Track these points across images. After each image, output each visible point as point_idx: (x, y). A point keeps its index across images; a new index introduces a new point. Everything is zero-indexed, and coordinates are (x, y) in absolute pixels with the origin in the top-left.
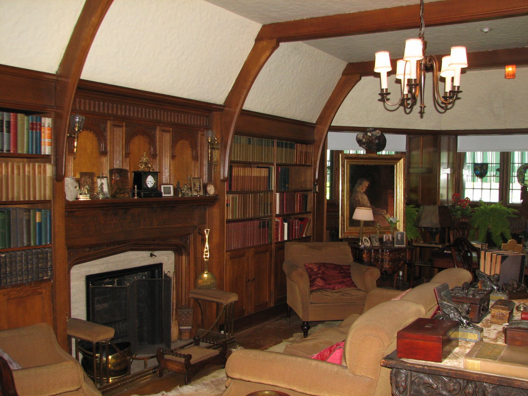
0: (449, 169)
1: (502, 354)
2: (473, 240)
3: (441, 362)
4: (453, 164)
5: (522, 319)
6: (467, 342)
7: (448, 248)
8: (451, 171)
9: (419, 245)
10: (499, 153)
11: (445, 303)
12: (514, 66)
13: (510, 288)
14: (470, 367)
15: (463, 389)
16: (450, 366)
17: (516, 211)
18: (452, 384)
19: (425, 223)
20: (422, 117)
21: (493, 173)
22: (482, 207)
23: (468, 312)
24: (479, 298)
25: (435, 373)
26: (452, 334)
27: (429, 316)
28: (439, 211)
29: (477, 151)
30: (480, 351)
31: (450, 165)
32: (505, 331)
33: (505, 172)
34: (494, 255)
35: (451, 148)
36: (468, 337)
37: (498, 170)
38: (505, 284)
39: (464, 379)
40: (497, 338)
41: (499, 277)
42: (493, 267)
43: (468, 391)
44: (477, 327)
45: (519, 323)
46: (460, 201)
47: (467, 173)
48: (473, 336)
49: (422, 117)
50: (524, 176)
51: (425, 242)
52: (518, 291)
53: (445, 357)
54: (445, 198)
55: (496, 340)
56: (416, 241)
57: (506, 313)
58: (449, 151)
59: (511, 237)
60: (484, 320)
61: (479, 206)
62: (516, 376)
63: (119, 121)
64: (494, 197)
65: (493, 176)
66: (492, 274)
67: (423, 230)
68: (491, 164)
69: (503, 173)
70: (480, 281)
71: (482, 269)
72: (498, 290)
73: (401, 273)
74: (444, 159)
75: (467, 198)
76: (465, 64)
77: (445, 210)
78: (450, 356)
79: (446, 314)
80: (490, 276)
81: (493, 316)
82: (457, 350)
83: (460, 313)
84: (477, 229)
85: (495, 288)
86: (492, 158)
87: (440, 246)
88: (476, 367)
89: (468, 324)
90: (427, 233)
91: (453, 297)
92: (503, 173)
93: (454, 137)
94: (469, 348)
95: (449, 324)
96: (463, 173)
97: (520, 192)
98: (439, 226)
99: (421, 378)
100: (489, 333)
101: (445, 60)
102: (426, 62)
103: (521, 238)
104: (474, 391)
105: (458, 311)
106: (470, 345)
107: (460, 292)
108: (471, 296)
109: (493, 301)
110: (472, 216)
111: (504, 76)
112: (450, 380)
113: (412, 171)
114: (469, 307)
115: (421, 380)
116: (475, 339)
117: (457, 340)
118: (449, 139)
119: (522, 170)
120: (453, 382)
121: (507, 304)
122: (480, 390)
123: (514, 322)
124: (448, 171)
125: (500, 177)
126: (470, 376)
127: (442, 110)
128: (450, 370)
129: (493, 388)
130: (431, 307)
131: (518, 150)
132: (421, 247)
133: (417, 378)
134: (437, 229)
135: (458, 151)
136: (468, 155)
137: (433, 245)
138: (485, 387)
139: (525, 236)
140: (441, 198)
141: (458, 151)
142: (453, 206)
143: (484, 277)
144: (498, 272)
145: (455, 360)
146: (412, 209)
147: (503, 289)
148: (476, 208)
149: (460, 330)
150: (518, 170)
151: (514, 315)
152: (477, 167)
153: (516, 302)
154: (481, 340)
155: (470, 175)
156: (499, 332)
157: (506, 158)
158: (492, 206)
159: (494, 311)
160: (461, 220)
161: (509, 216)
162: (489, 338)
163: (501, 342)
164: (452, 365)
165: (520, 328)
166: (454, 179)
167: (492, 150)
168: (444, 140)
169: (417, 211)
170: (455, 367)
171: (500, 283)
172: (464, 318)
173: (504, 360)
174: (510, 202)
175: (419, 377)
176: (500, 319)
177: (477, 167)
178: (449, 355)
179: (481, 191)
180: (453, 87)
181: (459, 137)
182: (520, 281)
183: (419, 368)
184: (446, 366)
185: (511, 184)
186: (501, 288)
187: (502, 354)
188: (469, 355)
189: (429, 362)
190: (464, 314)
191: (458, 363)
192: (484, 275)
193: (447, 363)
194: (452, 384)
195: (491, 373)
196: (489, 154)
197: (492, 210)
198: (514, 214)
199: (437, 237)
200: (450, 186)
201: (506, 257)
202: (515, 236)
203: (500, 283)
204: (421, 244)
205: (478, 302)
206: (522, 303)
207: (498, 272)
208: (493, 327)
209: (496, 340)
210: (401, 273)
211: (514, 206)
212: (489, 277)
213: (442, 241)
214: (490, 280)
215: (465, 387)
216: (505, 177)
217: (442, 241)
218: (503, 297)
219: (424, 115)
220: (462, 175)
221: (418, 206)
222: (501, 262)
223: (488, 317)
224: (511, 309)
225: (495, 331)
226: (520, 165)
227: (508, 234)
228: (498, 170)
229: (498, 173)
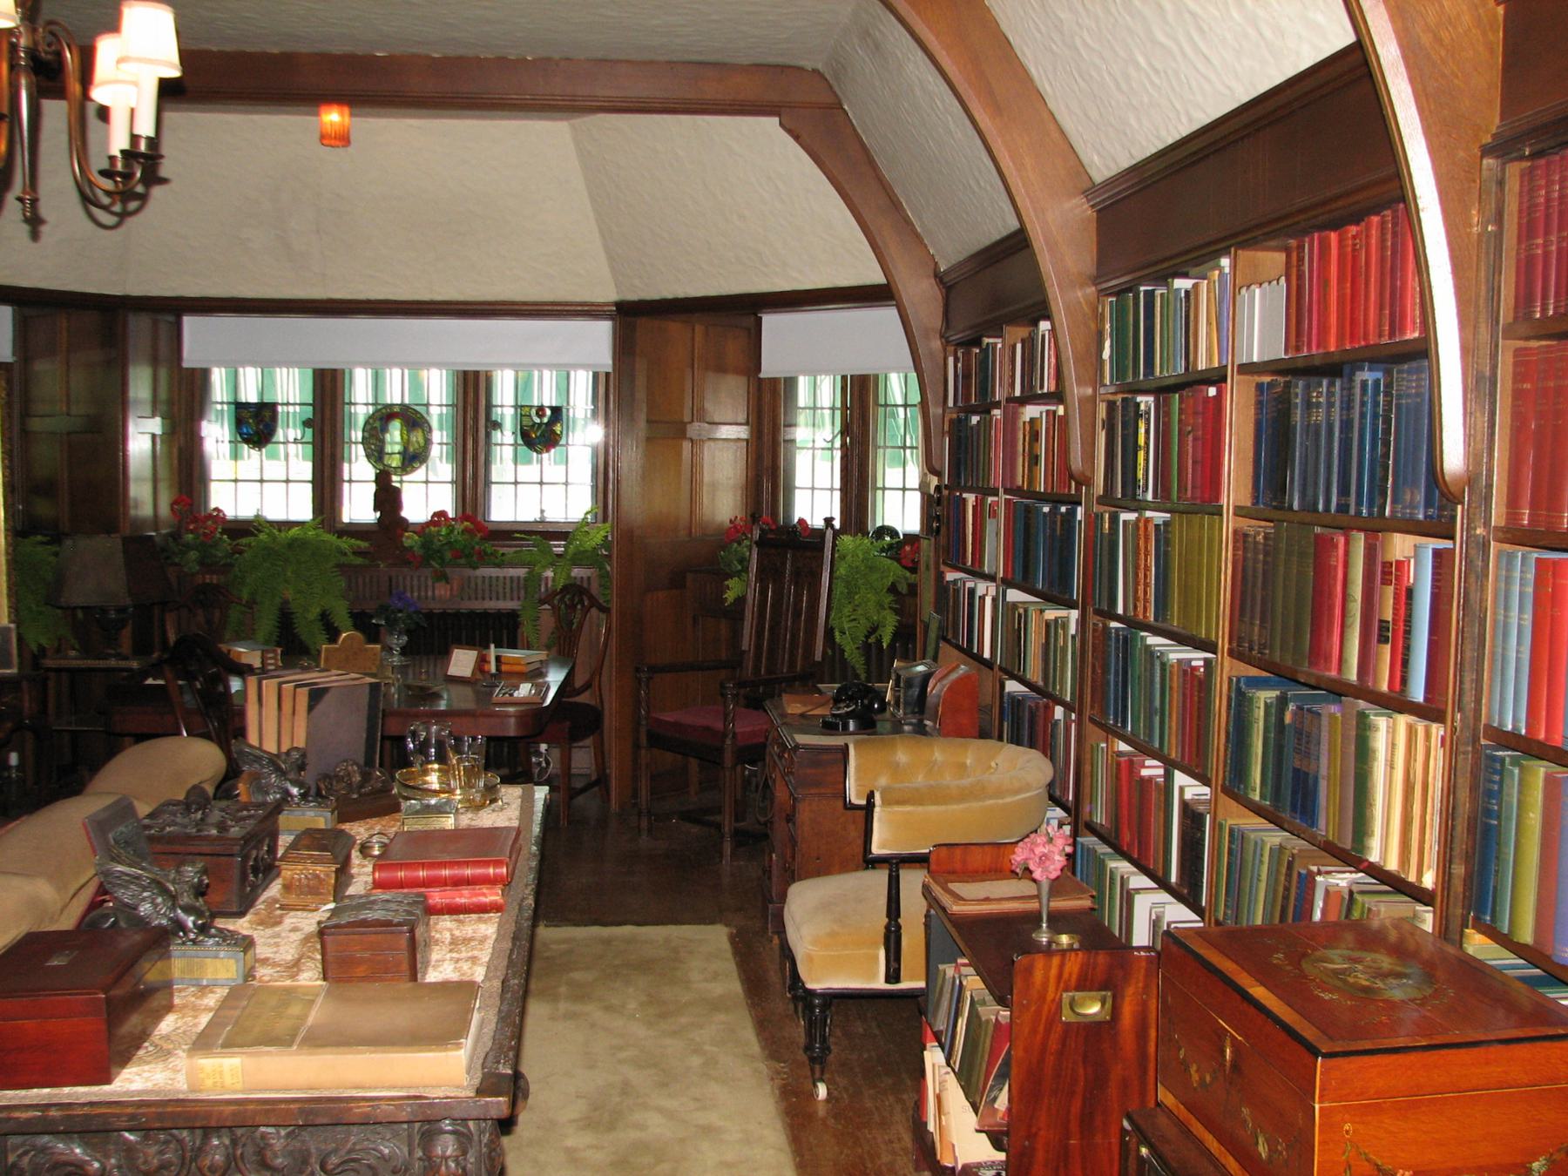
0: (158, 420)
1: (310, 1020)
2: (239, 637)
3: (108, 1081)
4: (170, 402)
5: (378, 885)
6: (204, 989)
7: (155, 670)
8: (163, 425)
9: (64, 663)
10: (310, 372)
11: (120, 868)
12: (346, 110)
13: (341, 788)
14: (209, 1083)
15: (194, 1159)
16: (139, 1092)
17: (364, 545)
18: (153, 1150)
19: (82, 593)
20: (35, 236)
21: (294, 433)
22: (262, 536)
23: (200, 891)
24: (243, 832)
25: (95, 1126)
26: (151, 973)
27: (67, 922)
28: (125, 552)
29: (244, 364)
30: (246, 1021)
31: (163, 408)
32: (322, 932)
33: (327, 429)
34: (288, 687)
35: (164, 350)
36: (201, 978)
37: (307, 423)
38: (326, 777)
39: (192, 1128)
40: (299, 960)
41: (304, 755)
42: (286, 725)
43: (208, 1162)
44: (233, 933)
45: (362, 907)
46: (195, 520)
47: (216, 434)
48: (222, 967)
49: (35, 236)
50: (383, 442)
51: (86, 651)
52: (367, 794)
53: (125, 1059)
54: (146, 510)
55: (295, 967)
56: (58, 651)
57: (326, 871)
58: (155, 362)
59: (349, 622)
60: (260, 905)
61: (252, 534)
62: (356, 1087)
63: (488, 435)
64: (297, 505)
65: (296, 441)
66: (284, 749)
67: (80, 614)
68: (288, 404)
69: (322, 432)
70: (244, 776)
71: (253, 739)
72: (304, 796)
73: (14, 759)
74: (140, 384)
75: (217, 509)
76: (170, 65)
77: (145, 551)
78: (141, 1052)
79: (127, 905)
80: (278, 756)
81: (287, 888)
82: (167, 1024)
83: (173, 898)
84: (251, 604)
85: (295, 791)
86: (291, 389)
87: (135, 665)
88: (228, 1080)
89: (203, 930)
90: (93, 626)
91: (151, 839)
92: (322, 432)
93: (171, 318)
94: (210, 1010)
95: (138, 937)
96: (203, 434)
97: (372, 487)
98: (128, 601)
99: (43, 1149)
100: (277, 945)
101: (106, 48)
102: (35, 43)
103: (378, 626)
104: (231, 1159)
105: (164, 891)
106: (211, 1000)
107: (179, 819)
108: (214, 832)
109: (290, 832)
110: (231, 565)
111: (317, 136)
112: (146, 1138)
113: (36, 424)
114: (205, 871)
115: (41, 1159)
116: (229, 975)
117: (167, 986)
118: (155, 323)
119: (377, 424)
120: (157, 1142)
121: (332, 846)
122: (250, 1149)
123: (347, 901)
124: (155, 425)
125: (314, 443)
126: (208, 1115)
127: (108, 219)
128: (141, 1104)
129: (288, 1135)
130: (82, 881)
131: (364, 365)
132: (72, 671)
133: (26, 1153)
134: (121, 610)
135: (185, 365)
136: (218, 377)
137: (113, 663)
138: (264, 1136)
139: (387, 619)
140: (132, 512)
141: (185, 365)
142: (175, 536)
143: (258, 759)
144: (300, 742)
145: (161, 1066)
146: (36, 547)
147: (319, 794)
148: (244, 541)
149: (175, 953)
150: (367, 423)
151: (354, 871)
152: (245, 414)
153: (359, 830)
154: (249, 975)
155: (227, 437)
156: (306, 939)
157: (328, 389)
158: (294, 531)
159: (289, 872)
160: (199, 580)
161: (343, 560)
162: (275, 964)
163: (310, 977)
164: (149, 1085)
165: (364, 923)
166: (175, 451)
167: (288, 364)
168: (138, 326)
169: (56, 554)
170: (158, 1093)
171: (308, 776)
172: (188, 910)
173: (318, 1040)
174: (346, 519)
175: (34, 1147)
176: (310, 893)
177: (245, 414)
178: (138, 1048)
179: (258, 487)
180: (135, 138)
181: (189, 322)
182: (369, 762)
183: (29, 1120)
184: (126, 1093)
185: (346, 466)
186: (313, 792)
187: (310, 1020)
188: (203, 1043)
189: (67, 1090)
190: (186, 899)
191: (168, 1074)
192: (259, 756)
193: (136, 1081)
194: (153, 1150)
195: (278, 1090)
196: (281, 374)
197: (293, 544)
198: (358, 553)
199: (126, 635)
200: (163, 473)
201: (326, 690)
202: (361, 621)
203: (308, 776)
204: (74, 659)
205: (237, 849)
206: (378, 828)
207: (300, 742)
208: (291, 920)
209: (295, 967)
210: (14, 759)
211: (356, 531)
212: (273, 761)
213: (141, 648)
214: (278, 769)
215: (199, 1151)
216: (328, 445)
217: (141, 648)
218: (319, 818)
219: (44, 229)
220: (201, 439)
221: (57, 538)
222: (311, 708)
223: (274, 889)
224: (341, 859)
225: (297, 936)
226: (371, 409)
227: (341, 616)
228: (307, 423)
229: (309, 432)
